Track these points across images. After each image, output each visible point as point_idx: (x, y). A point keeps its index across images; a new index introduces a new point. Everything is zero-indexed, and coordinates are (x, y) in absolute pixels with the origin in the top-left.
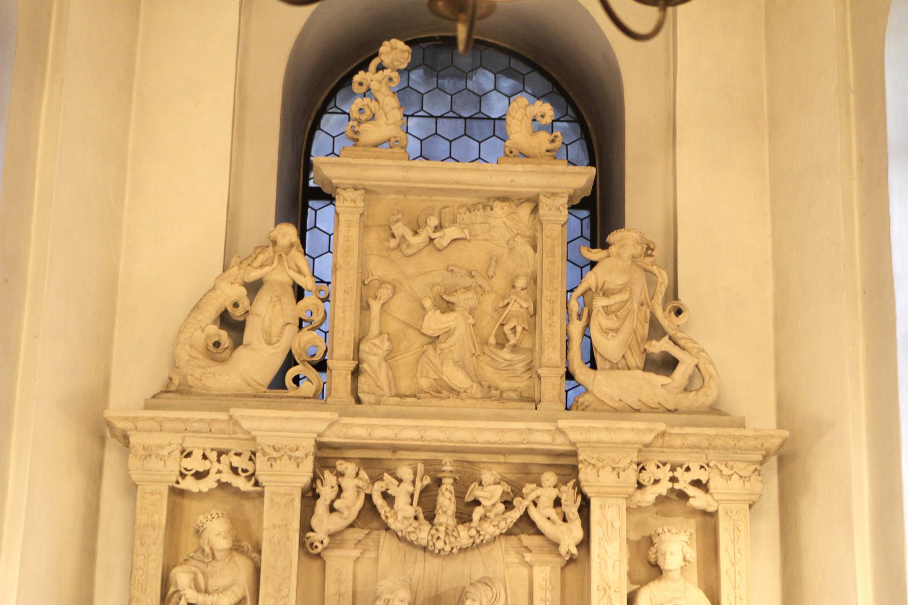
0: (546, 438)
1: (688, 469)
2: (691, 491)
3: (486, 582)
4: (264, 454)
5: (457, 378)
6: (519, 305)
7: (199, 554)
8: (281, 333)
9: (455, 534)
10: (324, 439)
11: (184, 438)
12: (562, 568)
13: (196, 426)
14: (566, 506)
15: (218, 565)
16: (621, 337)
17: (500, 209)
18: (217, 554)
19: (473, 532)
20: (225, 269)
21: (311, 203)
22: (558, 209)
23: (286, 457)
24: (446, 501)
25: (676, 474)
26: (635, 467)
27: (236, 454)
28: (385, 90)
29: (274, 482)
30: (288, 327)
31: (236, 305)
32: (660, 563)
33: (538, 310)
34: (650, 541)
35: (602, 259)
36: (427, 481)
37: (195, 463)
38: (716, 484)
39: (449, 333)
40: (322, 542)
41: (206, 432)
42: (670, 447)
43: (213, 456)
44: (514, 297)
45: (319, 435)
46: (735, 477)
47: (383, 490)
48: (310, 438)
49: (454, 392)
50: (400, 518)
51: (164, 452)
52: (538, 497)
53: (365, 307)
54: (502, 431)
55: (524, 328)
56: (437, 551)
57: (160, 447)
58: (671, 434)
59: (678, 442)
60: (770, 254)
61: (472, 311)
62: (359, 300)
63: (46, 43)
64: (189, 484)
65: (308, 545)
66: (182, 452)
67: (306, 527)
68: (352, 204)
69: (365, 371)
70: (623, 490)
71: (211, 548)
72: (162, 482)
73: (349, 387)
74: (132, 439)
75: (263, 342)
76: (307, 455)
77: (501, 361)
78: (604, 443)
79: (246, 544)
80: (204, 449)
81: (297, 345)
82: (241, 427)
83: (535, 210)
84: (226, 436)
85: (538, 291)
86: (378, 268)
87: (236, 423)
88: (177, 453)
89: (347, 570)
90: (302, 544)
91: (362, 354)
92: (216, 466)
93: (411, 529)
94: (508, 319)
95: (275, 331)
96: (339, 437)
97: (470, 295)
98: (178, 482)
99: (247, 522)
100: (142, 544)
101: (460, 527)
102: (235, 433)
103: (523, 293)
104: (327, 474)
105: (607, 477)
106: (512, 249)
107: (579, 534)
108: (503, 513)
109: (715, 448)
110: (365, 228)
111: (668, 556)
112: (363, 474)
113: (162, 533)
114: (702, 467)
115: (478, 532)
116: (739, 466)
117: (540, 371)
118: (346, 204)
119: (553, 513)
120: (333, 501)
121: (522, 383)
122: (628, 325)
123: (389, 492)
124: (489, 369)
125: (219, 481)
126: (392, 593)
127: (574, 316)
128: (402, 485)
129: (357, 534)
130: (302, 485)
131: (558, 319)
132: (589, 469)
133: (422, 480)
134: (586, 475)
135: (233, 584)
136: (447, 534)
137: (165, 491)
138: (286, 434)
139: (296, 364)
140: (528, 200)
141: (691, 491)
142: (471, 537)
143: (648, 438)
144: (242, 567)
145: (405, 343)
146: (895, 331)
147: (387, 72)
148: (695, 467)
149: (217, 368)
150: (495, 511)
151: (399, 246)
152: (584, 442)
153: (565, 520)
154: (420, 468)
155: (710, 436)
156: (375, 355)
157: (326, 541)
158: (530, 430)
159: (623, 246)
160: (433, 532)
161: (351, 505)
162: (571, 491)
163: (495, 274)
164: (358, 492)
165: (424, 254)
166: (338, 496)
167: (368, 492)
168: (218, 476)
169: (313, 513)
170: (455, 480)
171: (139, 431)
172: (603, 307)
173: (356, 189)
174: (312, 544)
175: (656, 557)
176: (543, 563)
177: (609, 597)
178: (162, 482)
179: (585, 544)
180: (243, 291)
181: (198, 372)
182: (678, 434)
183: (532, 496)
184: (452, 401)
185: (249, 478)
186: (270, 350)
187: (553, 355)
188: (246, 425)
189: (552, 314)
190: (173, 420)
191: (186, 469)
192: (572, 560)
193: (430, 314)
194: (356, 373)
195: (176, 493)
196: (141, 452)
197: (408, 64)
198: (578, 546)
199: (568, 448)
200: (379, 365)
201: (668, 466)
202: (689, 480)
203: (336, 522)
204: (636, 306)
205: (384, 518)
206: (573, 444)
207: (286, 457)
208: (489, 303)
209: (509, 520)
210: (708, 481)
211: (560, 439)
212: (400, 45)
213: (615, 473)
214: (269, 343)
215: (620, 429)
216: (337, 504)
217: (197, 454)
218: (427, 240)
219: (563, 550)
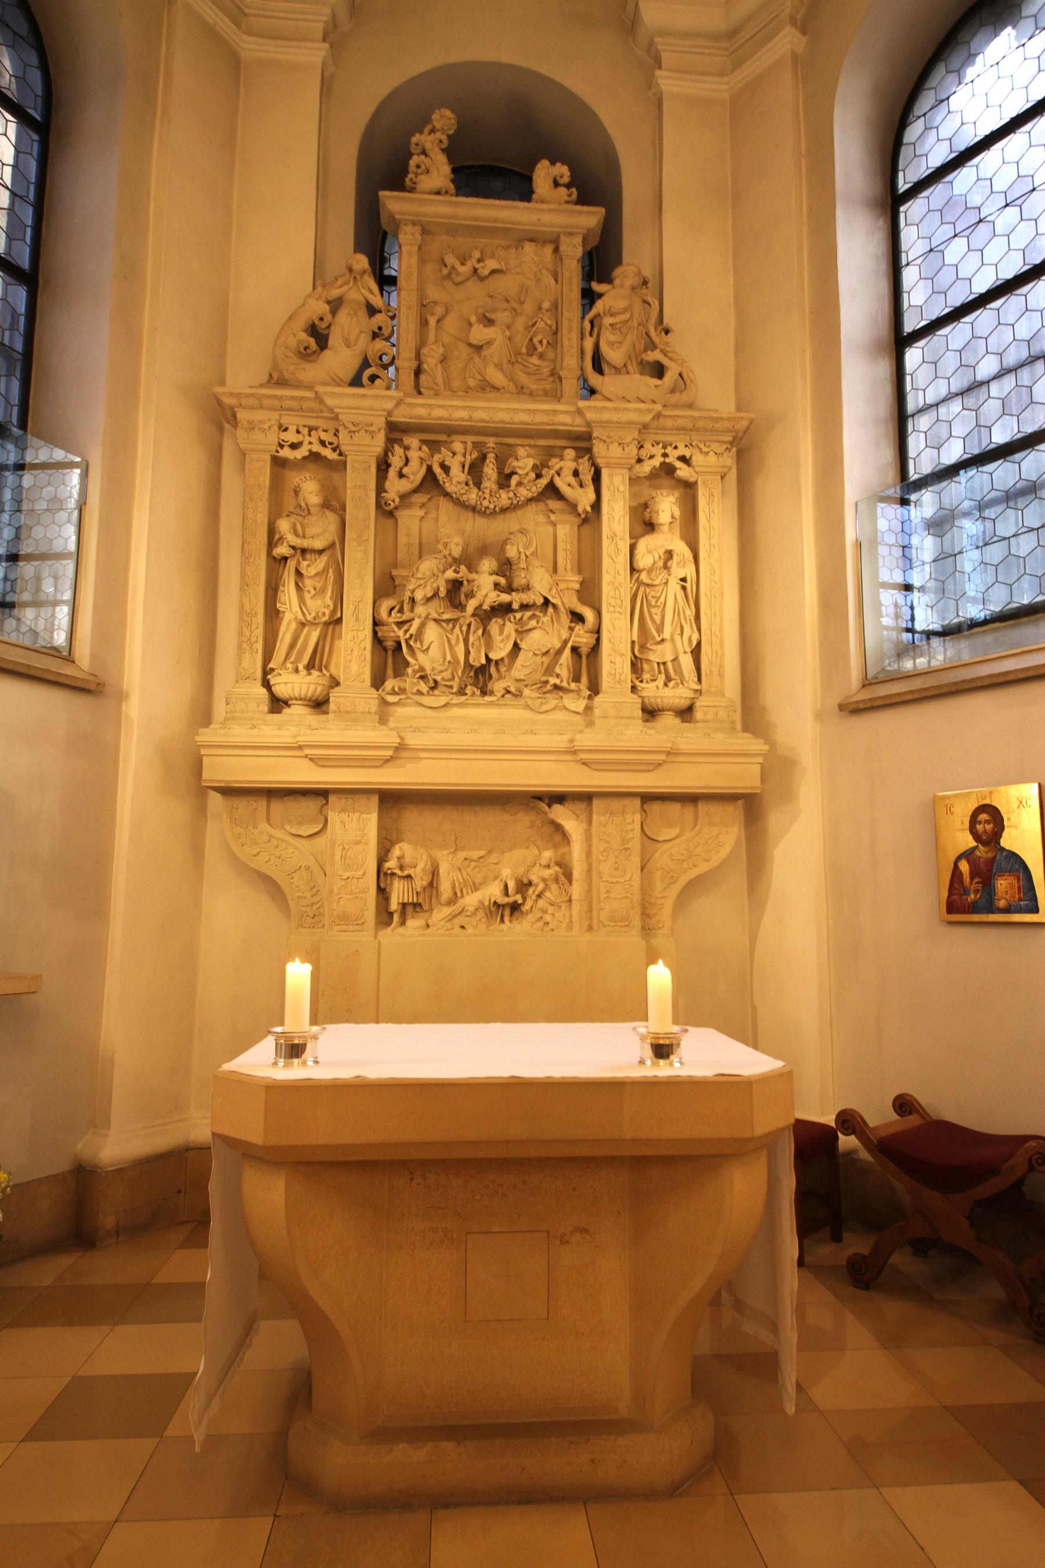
1: (676, 448)
3: (523, 532)
4: (345, 427)
5: (497, 378)
6: (544, 322)
7: (298, 510)
8: (357, 340)
9: (497, 495)
11: (281, 415)
13: (289, 404)
14: (583, 474)
15: (313, 518)
16: (625, 348)
17: (529, 248)
19: (511, 494)
20: (314, 288)
21: (385, 288)
22: (574, 246)
23: (363, 431)
24: (490, 470)
25: (667, 451)
26: (636, 443)
27: (323, 431)
28: (437, 150)
29: (354, 451)
30: (363, 334)
31: (321, 319)
32: (654, 521)
33: (559, 327)
34: (646, 506)
35: (607, 291)
37: (291, 437)
38: (697, 459)
39: (489, 343)
40: (394, 501)
41: (298, 411)
42: (664, 429)
43: (305, 431)
44: (541, 316)
45: (390, 414)
46: (712, 453)
47: (441, 461)
48: (380, 416)
51: (266, 426)
52: (561, 469)
53: (424, 323)
54: (534, 411)
55: (548, 342)
56: (483, 509)
58: (665, 416)
59: (669, 423)
60: (732, 299)
62: (419, 316)
64: (286, 453)
65: (383, 503)
67: (380, 489)
68: (411, 237)
69: (425, 371)
70: (627, 461)
71: (307, 505)
72: (265, 451)
73: (412, 383)
74: (239, 415)
75: (343, 344)
76: (379, 430)
77: (531, 366)
78: (613, 423)
79: (334, 503)
80: (298, 426)
81: (371, 352)
83: (556, 250)
84: (315, 415)
85: (559, 314)
86: (434, 293)
87: (322, 402)
88: (276, 428)
89: (415, 525)
90: (378, 505)
91: (422, 357)
92: (307, 439)
93: (463, 491)
95: (352, 338)
96: (405, 417)
97: (506, 313)
98: (278, 452)
99: (335, 488)
100: (251, 500)
101: (501, 491)
102: (322, 411)
103: (547, 314)
104: (396, 447)
105: (615, 451)
106: (538, 281)
107: (592, 496)
108: (535, 481)
109: (697, 430)
110: (422, 262)
111: (660, 513)
113: (267, 491)
114: (686, 446)
115: (515, 494)
116: (715, 446)
117: (561, 373)
118: (407, 236)
119: (572, 480)
120: (401, 469)
123: (446, 463)
124: (522, 374)
125: (310, 451)
126: (449, 538)
127: (587, 333)
128: (455, 457)
129: (421, 498)
130: (376, 454)
131: (575, 336)
132: (601, 444)
133: (471, 455)
134: (598, 449)
135: (325, 531)
136: (491, 495)
137: (268, 458)
138: (362, 412)
139: (370, 366)
140: (551, 242)
141: (678, 464)
142: (510, 499)
143: (647, 418)
145: (456, 353)
146: (840, 333)
147: (438, 135)
148: (681, 446)
149: (307, 366)
150: (528, 478)
152: (598, 422)
153: (581, 486)
154: (470, 445)
155: (694, 417)
156: (433, 357)
157: (397, 500)
158: (555, 411)
159: (625, 277)
160: (481, 493)
161: (416, 473)
162: (587, 463)
163: (525, 299)
164: (421, 463)
165: (470, 283)
166: (406, 464)
167: (429, 463)
168: (310, 447)
170: (497, 456)
171: (244, 408)
172: (610, 325)
173: (414, 224)
174: (386, 504)
175: (650, 516)
176: (565, 522)
177: (616, 544)
178: (265, 451)
179: (597, 506)
180: (327, 308)
181: (292, 368)
182: (670, 416)
183: (557, 467)
184: (493, 395)
185: (334, 450)
186: (349, 352)
189: (570, 330)
191: (283, 441)
193: (475, 327)
194: (418, 372)
195: (278, 463)
196: (246, 425)
197: (455, 131)
198: (592, 507)
200: (436, 365)
201: (661, 445)
202: (676, 456)
203: (405, 486)
204: (635, 324)
205: (442, 483)
207: (363, 431)
208: (520, 323)
209: (539, 486)
210: (690, 458)
211: (579, 420)
212: (448, 113)
213: (621, 447)
214: (349, 347)
216: (405, 471)
217: (292, 429)
218: (472, 269)
219: (580, 509)
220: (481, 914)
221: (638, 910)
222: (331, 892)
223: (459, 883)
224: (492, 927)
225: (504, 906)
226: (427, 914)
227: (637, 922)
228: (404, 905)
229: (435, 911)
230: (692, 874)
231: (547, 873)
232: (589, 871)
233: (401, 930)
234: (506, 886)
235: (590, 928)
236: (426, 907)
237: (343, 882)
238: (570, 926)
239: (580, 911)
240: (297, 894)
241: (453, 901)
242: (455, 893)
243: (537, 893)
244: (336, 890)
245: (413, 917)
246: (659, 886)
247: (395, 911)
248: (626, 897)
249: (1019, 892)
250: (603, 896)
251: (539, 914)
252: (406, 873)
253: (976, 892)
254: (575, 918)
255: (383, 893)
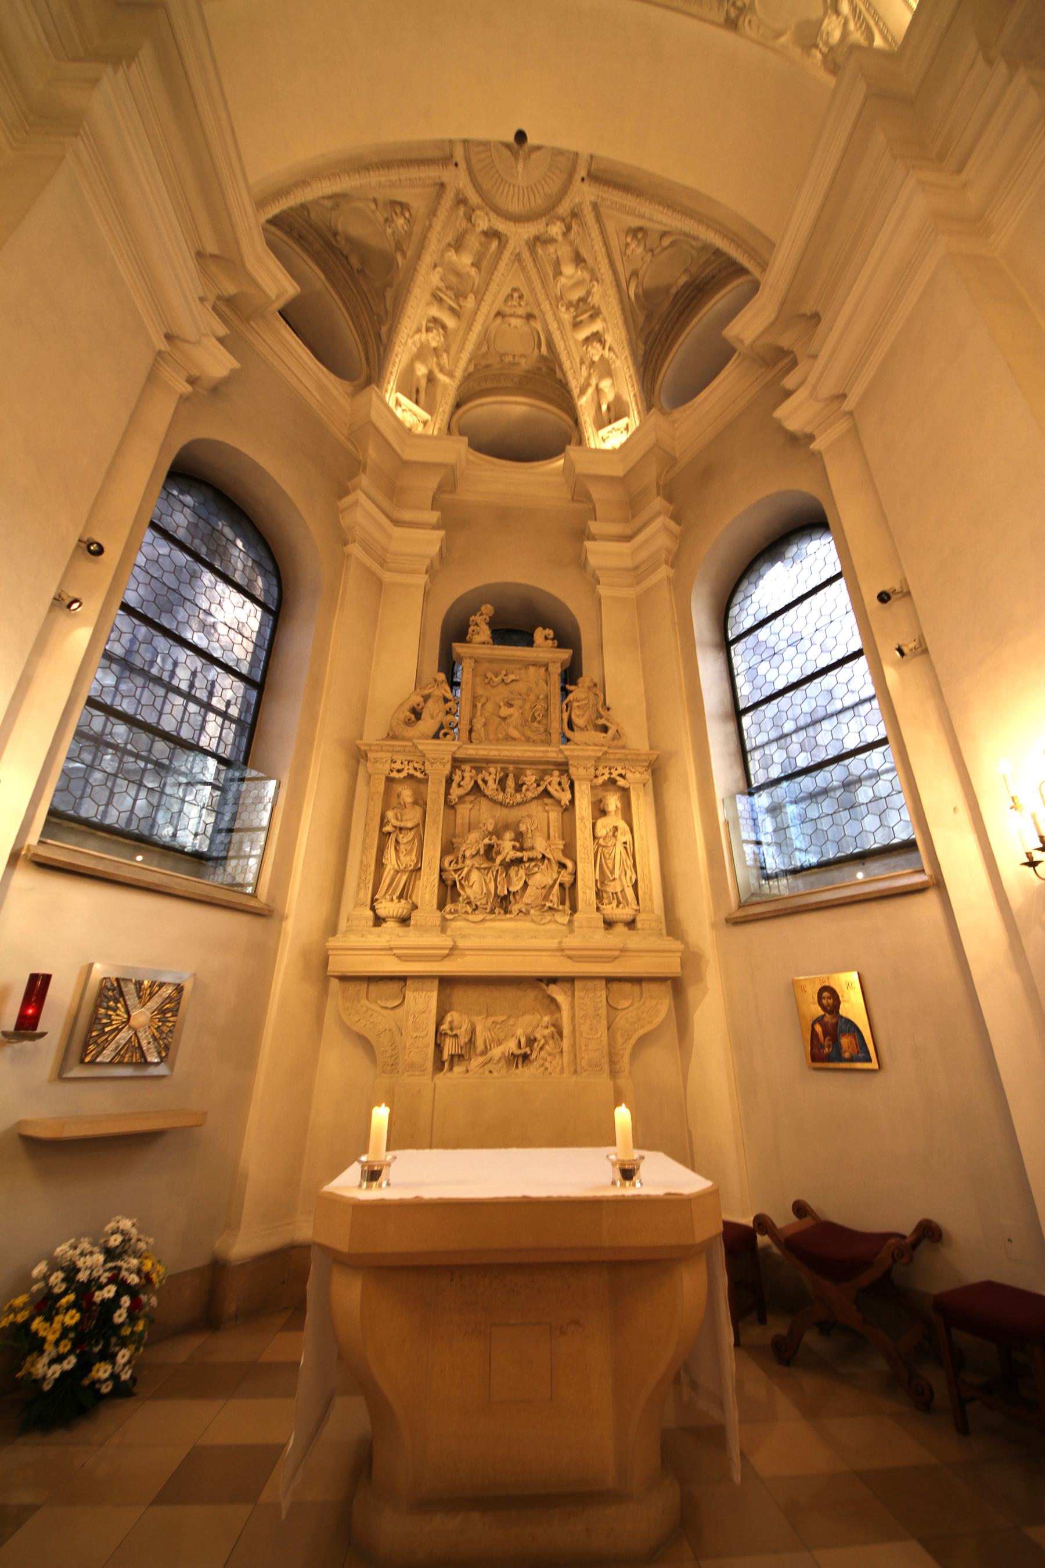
0: (555, 755)
2: (618, 778)
3: (530, 816)
4: (429, 761)
5: (515, 733)
7: (399, 806)
8: (437, 715)
10: (456, 756)
12: (562, 813)
13: (398, 749)
15: (407, 811)
16: (586, 717)
17: (532, 669)
18: (407, 805)
19: (523, 796)
24: (510, 782)
31: (418, 705)
32: (606, 809)
34: (601, 801)
36: (502, 774)
37: (398, 766)
38: (629, 775)
39: (511, 716)
45: (454, 753)
49: (514, 739)
50: (490, 789)
51: (384, 760)
53: (475, 706)
57: (382, 758)
58: (609, 753)
61: (521, 708)
63: (337, 597)
64: (395, 775)
66: (392, 761)
67: (447, 793)
74: (369, 755)
82: (418, 749)
83: (547, 670)
86: (480, 691)
88: (389, 761)
92: (407, 767)
94: (536, 711)
95: (435, 715)
97: (520, 701)
105: (582, 771)
107: (569, 796)
109: (628, 760)
110: (474, 676)
112: (473, 771)
119: (558, 788)
120: (459, 782)
121: (543, 737)
122: (587, 713)
125: (408, 774)
129: (471, 798)
131: (558, 711)
135: (414, 818)
140: (544, 666)
141: (618, 778)
143: (600, 754)
144: (418, 811)
146: (704, 710)
147: (484, 616)
151: (489, 683)
153: (563, 790)
157: (457, 800)
158: (547, 751)
161: (468, 784)
169: (451, 787)
177: (584, 823)
179: (572, 801)
180: (422, 699)
183: (549, 781)
185: (422, 772)
186: (433, 721)
187: (555, 725)
188: (420, 747)
190: (387, 745)
192: (566, 809)
194: (471, 731)
195: (390, 780)
196: (373, 760)
199: (564, 760)
203: (461, 791)
206: (566, 757)
208: (527, 706)
211: (561, 756)
215: (587, 750)
216: (462, 783)
217: (399, 762)
219: (563, 803)
220: (503, 1062)
221: (606, 1059)
222: (404, 1047)
223: (489, 1040)
224: (510, 1072)
225: (518, 1056)
226: (467, 1062)
227: (606, 1067)
228: (452, 1056)
229: (472, 1060)
230: (641, 1032)
231: (546, 1032)
232: (574, 1030)
233: (449, 1075)
234: (519, 1042)
235: (575, 1072)
236: (466, 1057)
237: (412, 1040)
238: (562, 1071)
239: (568, 1060)
240: (382, 1049)
241: (484, 1053)
242: (486, 1047)
243: (540, 1046)
244: (408, 1046)
245: (458, 1065)
246: (620, 1041)
247: (446, 1061)
248: (598, 1049)
249: (857, 1048)
250: (584, 1048)
251: (541, 1062)
252: (454, 1033)
253: (829, 1047)
254: (565, 1064)
255: (439, 1047)
